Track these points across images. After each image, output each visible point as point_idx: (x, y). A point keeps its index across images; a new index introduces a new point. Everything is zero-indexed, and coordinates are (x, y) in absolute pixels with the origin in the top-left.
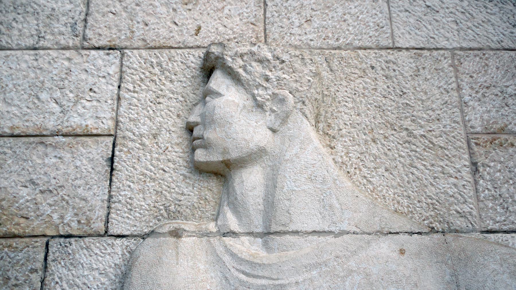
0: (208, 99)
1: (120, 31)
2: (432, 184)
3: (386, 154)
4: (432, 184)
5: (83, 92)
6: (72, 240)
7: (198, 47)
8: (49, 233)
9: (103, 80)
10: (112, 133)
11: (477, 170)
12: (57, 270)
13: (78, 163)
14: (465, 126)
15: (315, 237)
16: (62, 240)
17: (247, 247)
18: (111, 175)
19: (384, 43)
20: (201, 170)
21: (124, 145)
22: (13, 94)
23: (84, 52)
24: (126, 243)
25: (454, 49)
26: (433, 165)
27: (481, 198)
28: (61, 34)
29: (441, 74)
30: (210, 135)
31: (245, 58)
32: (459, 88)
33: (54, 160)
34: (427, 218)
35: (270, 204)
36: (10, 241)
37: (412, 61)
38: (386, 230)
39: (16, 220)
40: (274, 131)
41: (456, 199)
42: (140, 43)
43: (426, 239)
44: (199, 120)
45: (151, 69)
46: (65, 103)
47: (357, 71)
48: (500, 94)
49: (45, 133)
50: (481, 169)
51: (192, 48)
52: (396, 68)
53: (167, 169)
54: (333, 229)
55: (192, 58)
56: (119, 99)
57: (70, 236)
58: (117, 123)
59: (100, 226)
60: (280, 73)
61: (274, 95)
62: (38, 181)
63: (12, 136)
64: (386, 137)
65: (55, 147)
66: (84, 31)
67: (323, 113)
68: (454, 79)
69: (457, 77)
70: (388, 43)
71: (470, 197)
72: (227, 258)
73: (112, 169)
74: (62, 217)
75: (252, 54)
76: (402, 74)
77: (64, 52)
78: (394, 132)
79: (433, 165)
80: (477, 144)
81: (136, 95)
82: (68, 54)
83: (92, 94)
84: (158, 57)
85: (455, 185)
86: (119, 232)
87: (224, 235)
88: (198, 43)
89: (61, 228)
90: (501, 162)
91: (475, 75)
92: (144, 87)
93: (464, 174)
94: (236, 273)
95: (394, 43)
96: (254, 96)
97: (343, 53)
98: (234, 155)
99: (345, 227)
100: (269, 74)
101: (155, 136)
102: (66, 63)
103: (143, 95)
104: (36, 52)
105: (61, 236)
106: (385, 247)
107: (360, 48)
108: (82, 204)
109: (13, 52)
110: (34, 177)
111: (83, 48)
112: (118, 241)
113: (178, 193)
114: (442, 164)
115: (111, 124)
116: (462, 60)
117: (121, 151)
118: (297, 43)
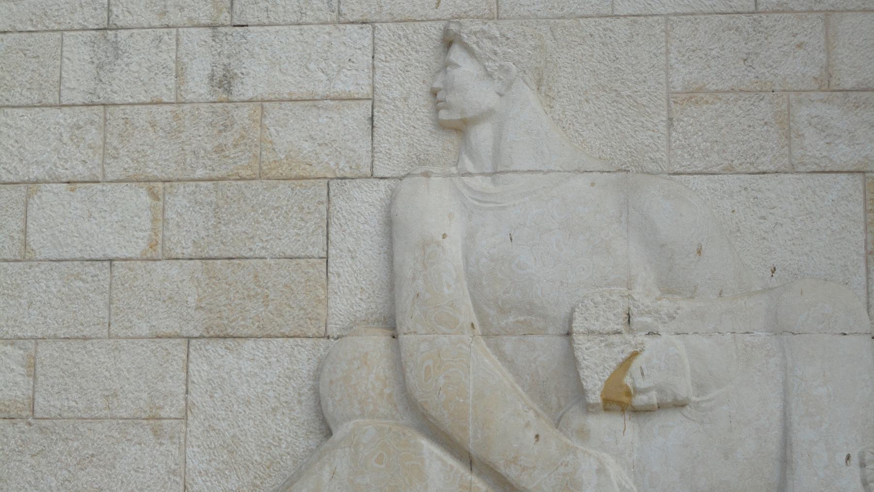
0: (448, 68)
1: (370, 6)
2: (632, 136)
3: (596, 112)
4: (632, 136)
5: (344, 62)
6: (347, 181)
7: (439, 20)
8: (329, 175)
9: (359, 52)
10: (371, 97)
11: (672, 124)
12: (338, 202)
13: (346, 122)
14: (668, 86)
15: (529, 175)
16: (339, 181)
17: (479, 183)
18: (372, 131)
19: (604, 11)
20: (443, 127)
21: (381, 107)
22: (286, 65)
23: (341, 26)
24: (388, 183)
25: (669, 14)
26: (635, 121)
27: (673, 147)
28: (320, 10)
29: (653, 39)
30: (451, 98)
31: (478, 35)
32: (668, 52)
33: (326, 120)
34: (625, 163)
35: (497, 152)
36: (300, 182)
37: (627, 27)
38: (582, 169)
39: (303, 166)
40: (501, 95)
41: (651, 148)
42: (388, 17)
43: (613, 176)
44: (442, 86)
45: (399, 41)
46: (329, 72)
47: (577, 39)
48: (704, 56)
49: (316, 98)
50: (675, 124)
51: (433, 20)
52: (611, 35)
53: (417, 126)
54: (542, 168)
55: (433, 30)
56: (374, 68)
57: (345, 178)
58: (374, 89)
59: (367, 170)
60: (505, 48)
61: (501, 66)
62: (315, 137)
63: (291, 100)
64: (597, 98)
65: (326, 109)
66: (339, 7)
67: (546, 77)
68: (664, 44)
69: (667, 42)
70: (608, 10)
71: (663, 147)
72: (464, 191)
73: (373, 127)
74: (337, 164)
75: (484, 32)
76: (617, 41)
77: (324, 27)
78: (605, 93)
79: (635, 121)
80: (675, 102)
81: (387, 64)
82: (327, 28)
83: (351, 64)
84: (404, 30)
85: (651, 137)
86: (382, 175)
87: (463, 175)
88: (438, 16)
89: (337, 172)
90: (693, 117)
91: (684, 40)
92: (394, 57)
93: (660, 127)
94: (472, 201)
95: (613, 11)
96: (485, 67)
97: (566, 22)
98: (470, 114)
99: (552, 167)
100: (497, 49)
101: (405, 99)
102: (327, 37)
103: (393, 64)
104: (301, 27)
105: (338, 178)
106: (581, 182)
107: (582, 17)
108: (351, 154)
109: (281, 28)
110: (313, 133)
111: (340, 23)
112: (382, 182)
113: (426, 145)
114: (642, 119)
115: (368, 89)
116: (674, 25)
117: (379, 112)
118: (526, 14)
